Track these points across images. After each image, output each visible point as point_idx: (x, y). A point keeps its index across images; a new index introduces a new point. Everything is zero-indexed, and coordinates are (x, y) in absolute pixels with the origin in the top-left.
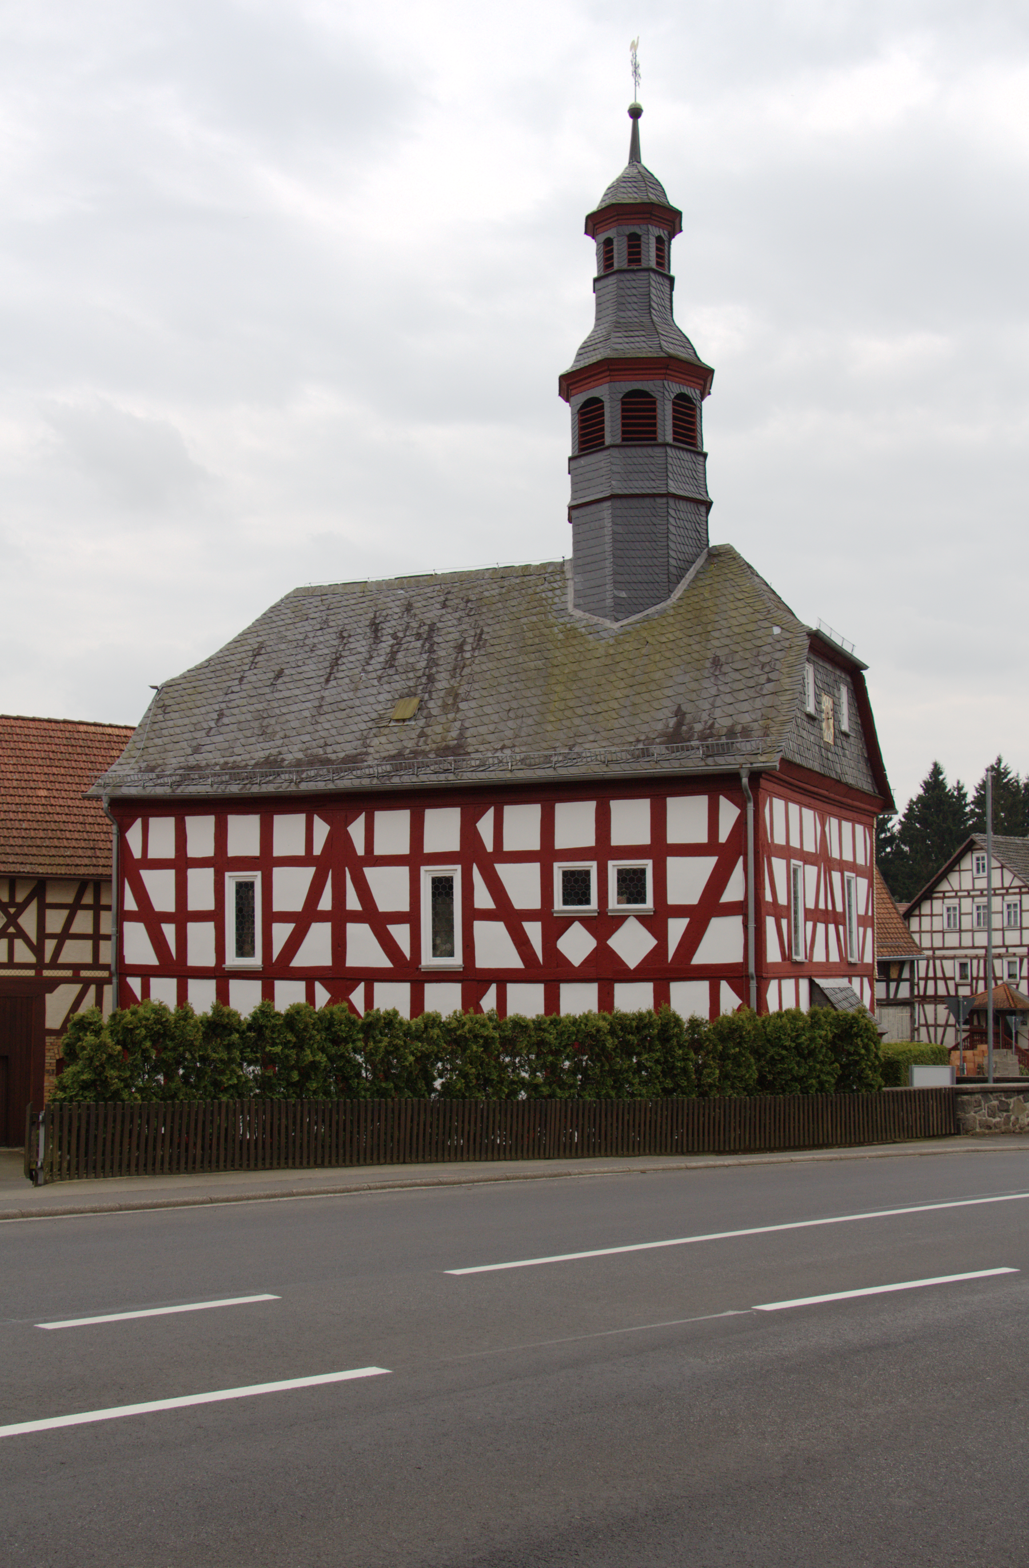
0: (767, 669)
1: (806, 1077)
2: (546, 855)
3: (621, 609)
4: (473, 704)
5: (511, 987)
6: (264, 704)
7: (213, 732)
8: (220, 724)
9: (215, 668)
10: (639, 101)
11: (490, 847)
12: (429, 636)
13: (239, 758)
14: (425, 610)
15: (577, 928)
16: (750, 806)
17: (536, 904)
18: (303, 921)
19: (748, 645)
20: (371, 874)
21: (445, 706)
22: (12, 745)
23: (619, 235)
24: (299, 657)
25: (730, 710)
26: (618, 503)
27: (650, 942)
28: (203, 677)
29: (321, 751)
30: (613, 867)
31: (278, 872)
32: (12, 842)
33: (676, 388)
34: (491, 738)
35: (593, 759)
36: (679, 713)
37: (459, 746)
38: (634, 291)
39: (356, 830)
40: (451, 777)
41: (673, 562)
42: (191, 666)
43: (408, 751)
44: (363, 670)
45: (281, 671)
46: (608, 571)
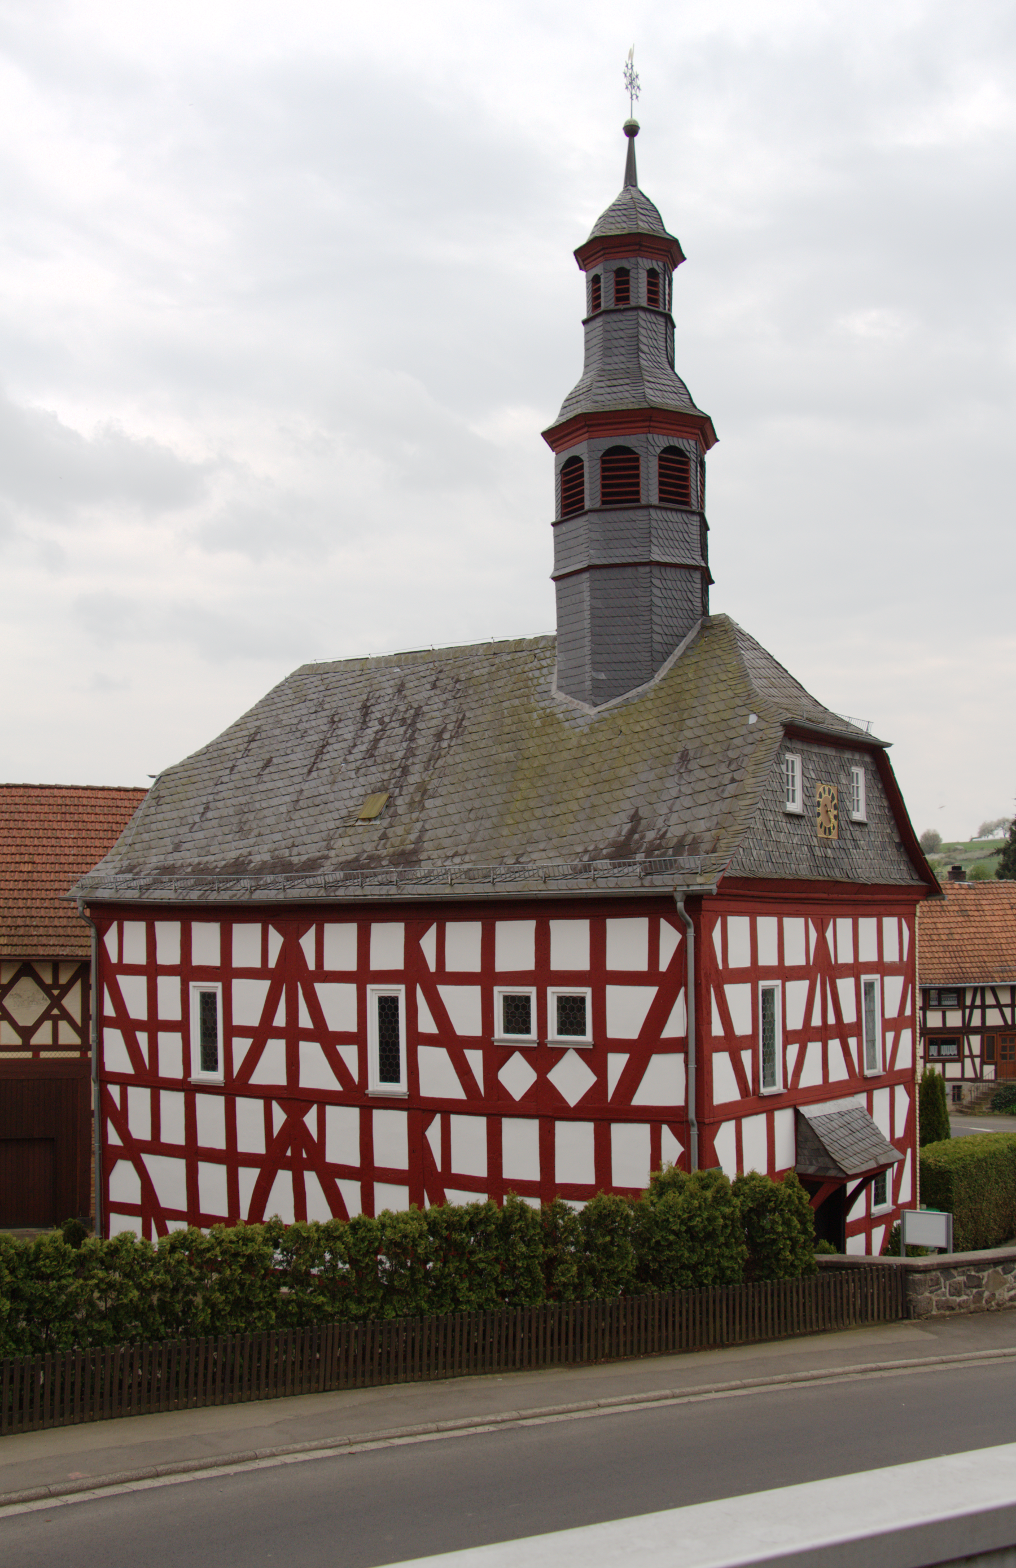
0: (733, 767)
1: (701, 1263)
2: (487, 977)
3: (599, 693)
4: (438, 802)
5: (454, 1119)
6: (247, 797)
7: (196, 828)
8: (204, 819)
9: (212, 755)
10: (635, 118)
11: (433, 968)
12: (411, 723)
13: (212, 858)
14: (415, 690)
15: (517, 1058)
16: (691, 933)
17: (477, 1031)
18: (261, 1034)
19: (721, 737)
20: (322, 989)
21: (411, 804)
22: (76, 817)
23: (606, 271)
24: (289, 744)
25: (686, 815)
26: (597, 574)
27: (590, 1079)
28: (199, 765)
29: (287, 852)
30: (553, 993)
31: (237, 984)
32: (56, 922)
33: (662, 441)
34: (447, 842)
35: (547, 871)
36: (635, 818)
37: (415, 852)
38: (621, 334)
39: (307, 942)
40: (393, 890)
41: (657, 638)
42: (191, 752)
43: (365, 855)
44: (345, 760)
45: (270, 760)
46: (587, 650)
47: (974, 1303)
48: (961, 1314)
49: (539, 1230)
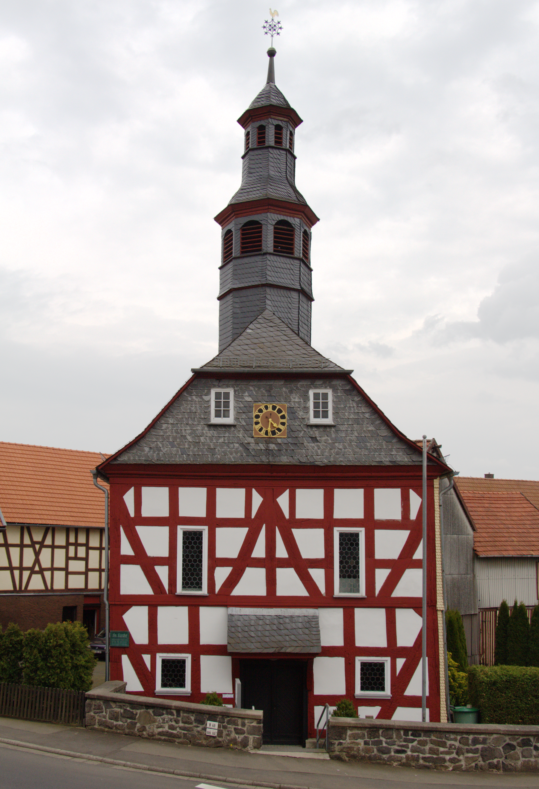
2: (328, 523)
11: (132, 514)
47: (129, 728)
48: (117, 733)
49: (32, 658)
